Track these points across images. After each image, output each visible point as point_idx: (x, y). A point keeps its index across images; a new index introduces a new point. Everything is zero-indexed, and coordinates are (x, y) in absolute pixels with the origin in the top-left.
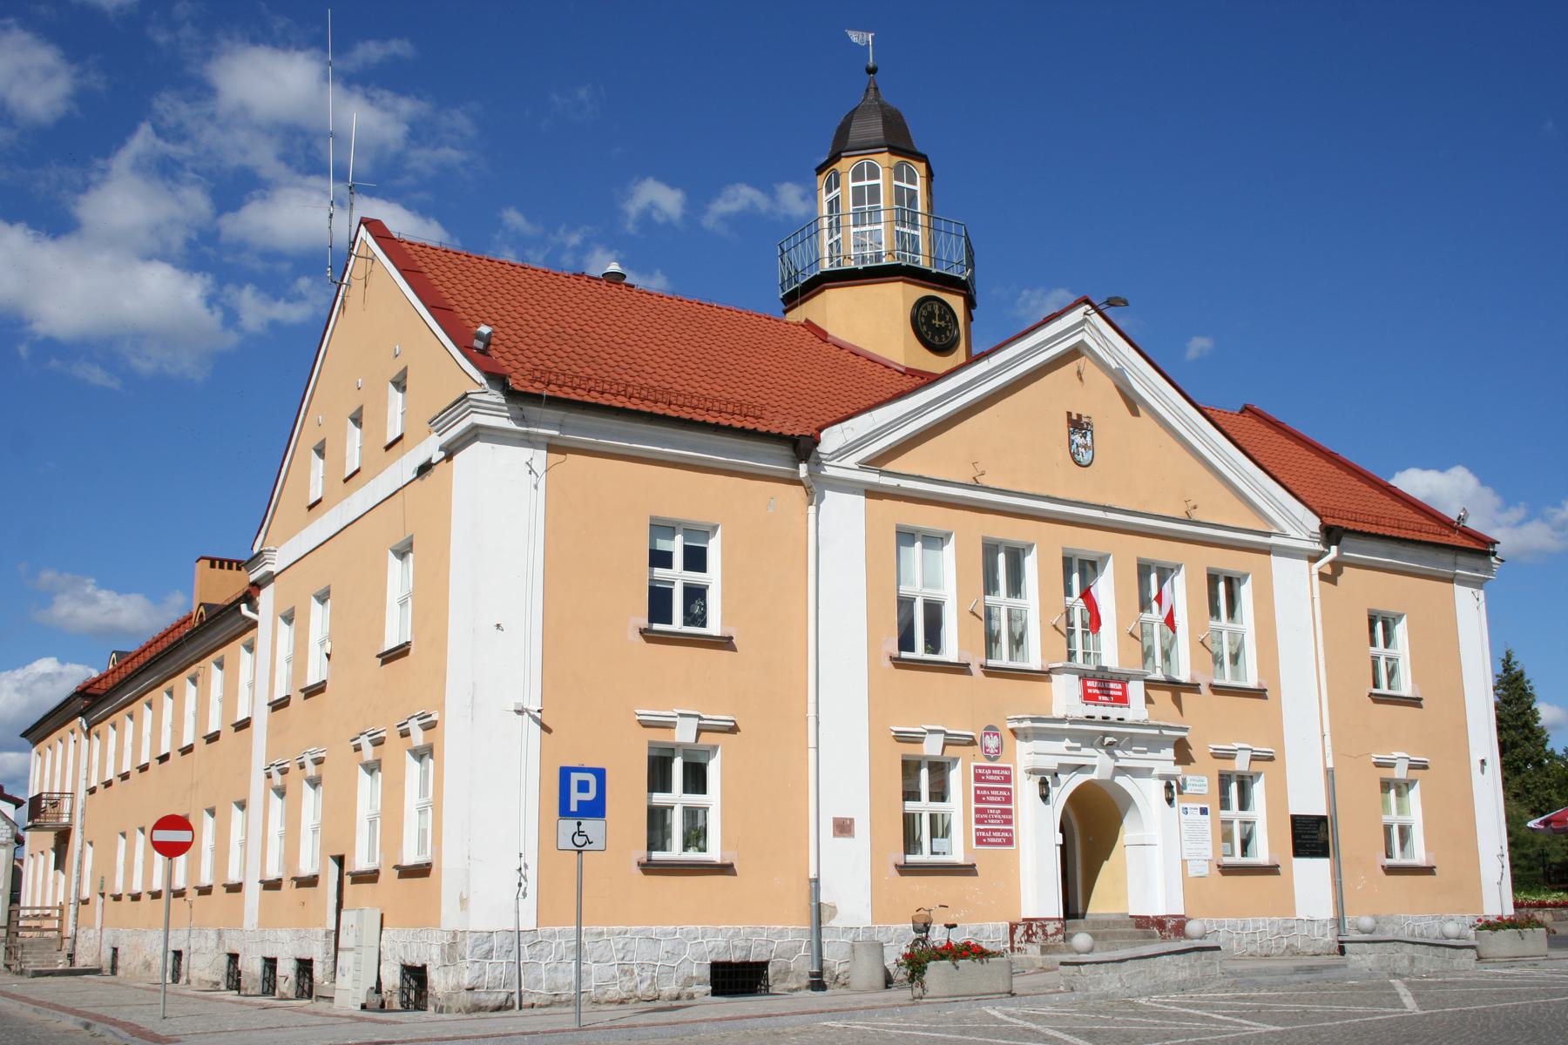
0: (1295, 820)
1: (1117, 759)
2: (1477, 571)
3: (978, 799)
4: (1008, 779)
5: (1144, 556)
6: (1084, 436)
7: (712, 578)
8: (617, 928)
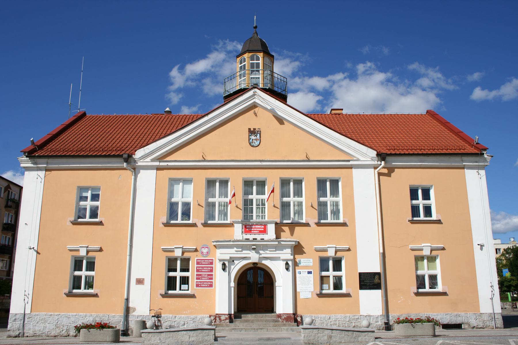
0: (360, 274)
1: (260, 254)
2: (477, 162)
4: (212, 263)
5: (318, 176)
6: (256, 136)
7: (432, 202)
8: (56, 313)
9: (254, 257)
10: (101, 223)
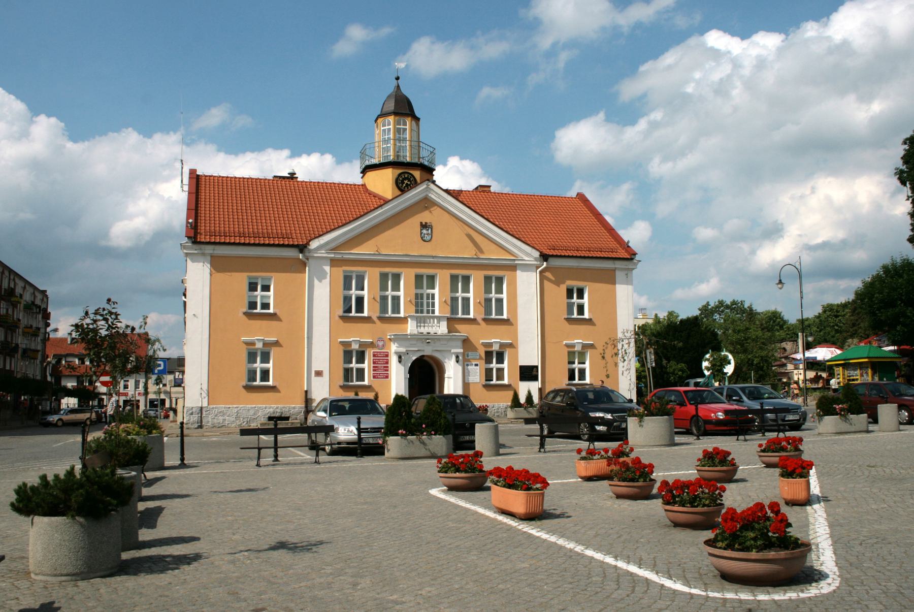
0: (521, 367)
3: (374, 363)
4: (387, 356)
9: (428, 351)
10: (273, 388)
